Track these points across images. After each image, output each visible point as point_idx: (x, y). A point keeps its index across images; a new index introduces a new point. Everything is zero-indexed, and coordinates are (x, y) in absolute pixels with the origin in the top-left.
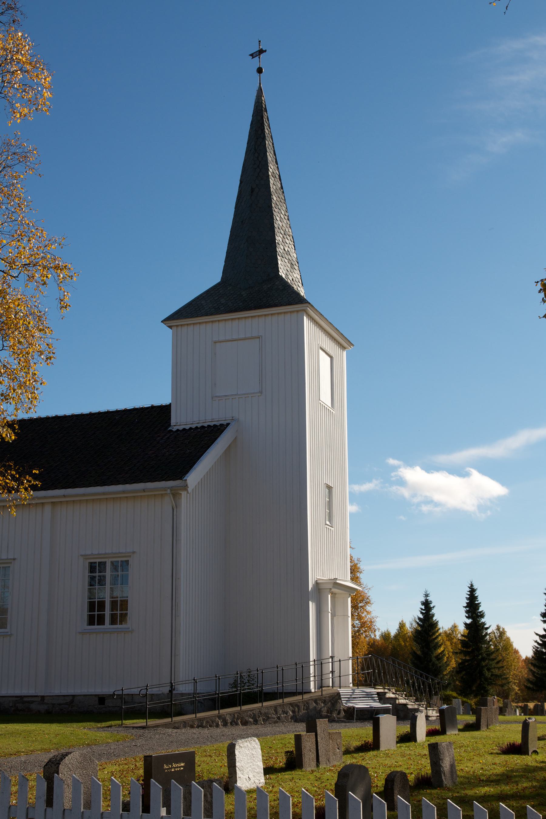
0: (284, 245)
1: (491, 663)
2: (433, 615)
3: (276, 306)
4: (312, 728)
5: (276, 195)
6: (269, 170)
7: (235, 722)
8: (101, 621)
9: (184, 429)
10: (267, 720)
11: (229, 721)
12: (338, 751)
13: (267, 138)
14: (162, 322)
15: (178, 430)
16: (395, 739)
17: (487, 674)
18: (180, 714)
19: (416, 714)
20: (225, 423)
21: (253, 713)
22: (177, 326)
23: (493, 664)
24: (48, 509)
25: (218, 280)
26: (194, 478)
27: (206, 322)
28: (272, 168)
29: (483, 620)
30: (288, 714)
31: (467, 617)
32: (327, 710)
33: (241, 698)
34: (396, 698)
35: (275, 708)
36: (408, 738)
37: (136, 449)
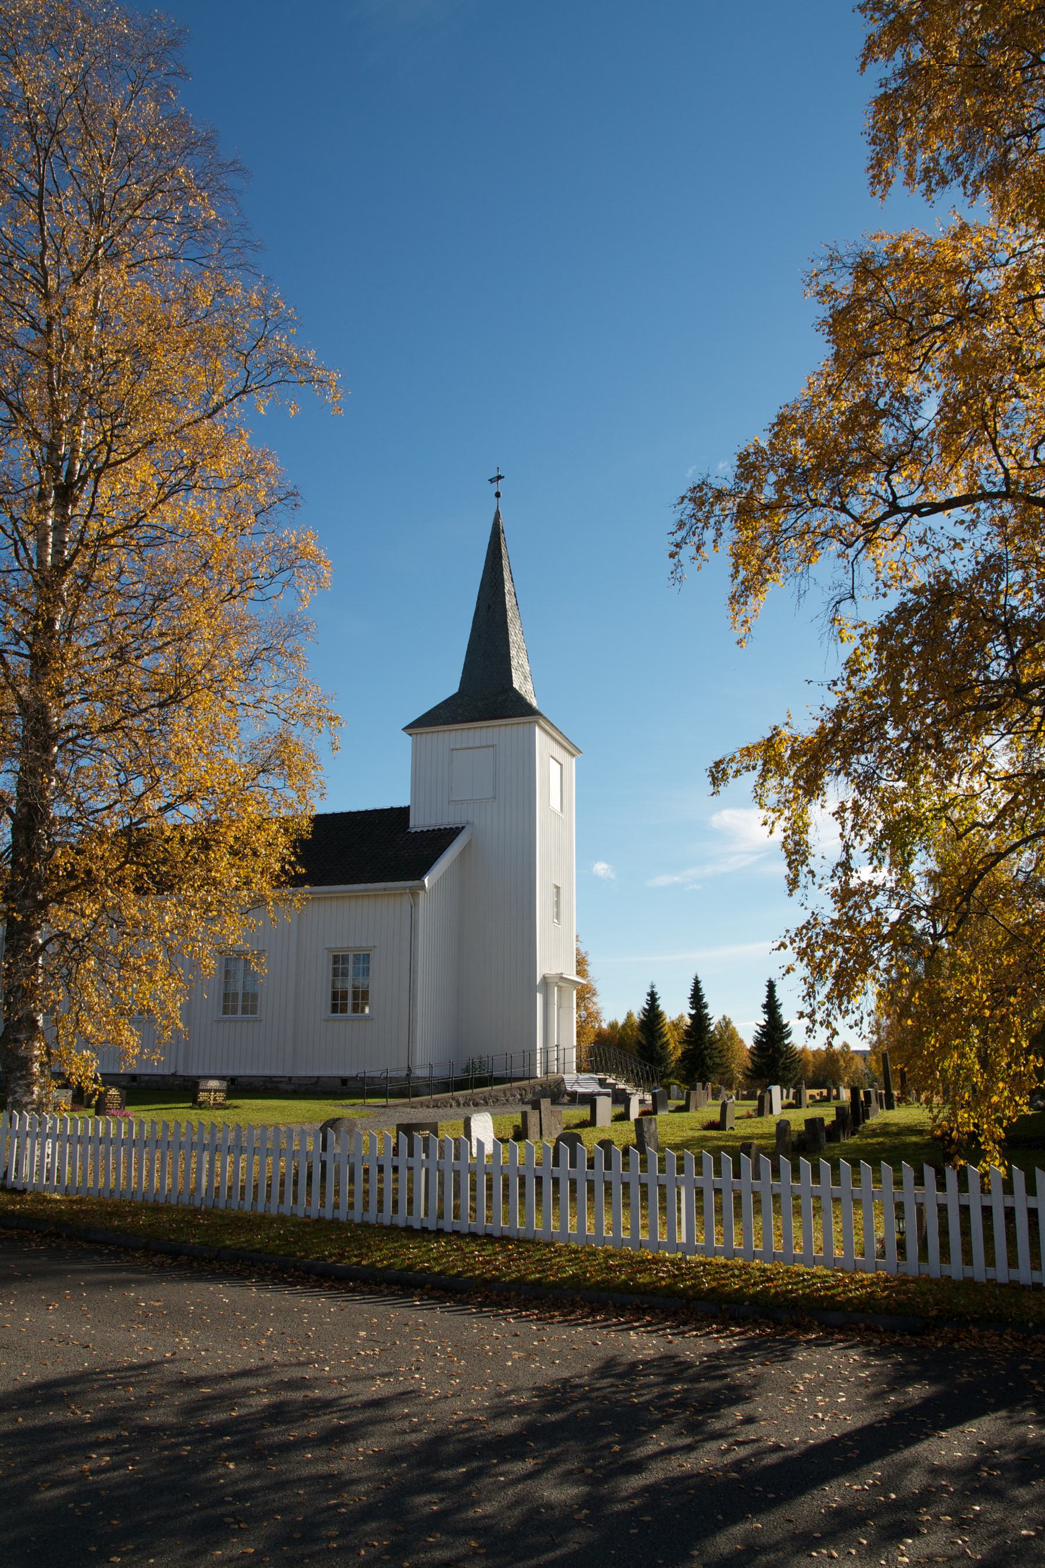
0: (519, 659)
3: (510, 717)
4: (536, 1106)
8: (344, 1010)
11: (462, 1102)
16: (610, 1118)
17: (709, 1062)
20: (460, 826)
23: (715, 1053)
28: (508, 586)
33: (473, 1080)
36: (623, 1117)
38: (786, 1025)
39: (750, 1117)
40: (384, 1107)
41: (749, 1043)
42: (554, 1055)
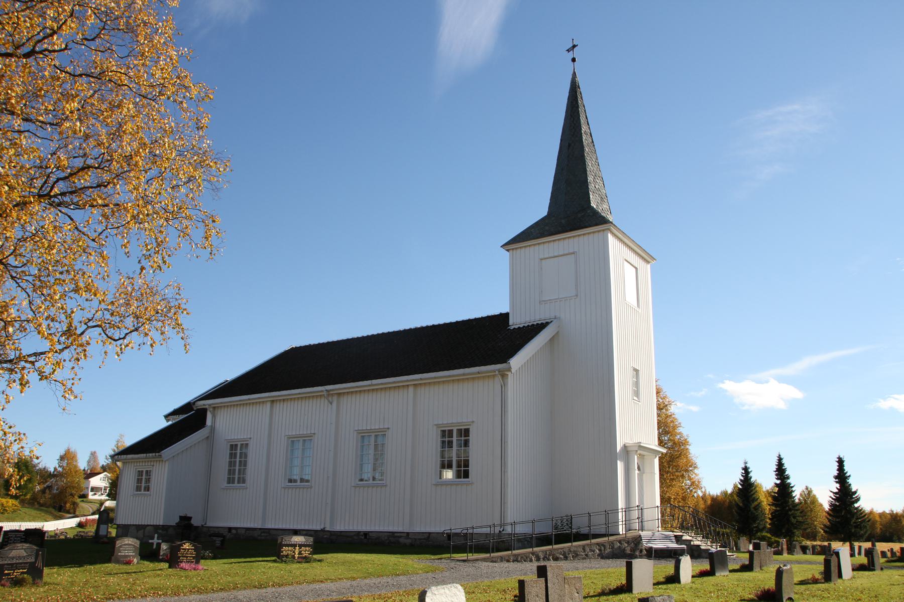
11: (542, 557)
17: (793, 521)
18: (498, 550)
23: (798, 513)
24: (411, 389)
26: (516, 362)
28: (584, 128)
29: (789, 481)
37: (483, 343)
38: (855, 492)
39: (815, 581)
40: (464, 561)
41: (827, 507)
42: (635, 514)
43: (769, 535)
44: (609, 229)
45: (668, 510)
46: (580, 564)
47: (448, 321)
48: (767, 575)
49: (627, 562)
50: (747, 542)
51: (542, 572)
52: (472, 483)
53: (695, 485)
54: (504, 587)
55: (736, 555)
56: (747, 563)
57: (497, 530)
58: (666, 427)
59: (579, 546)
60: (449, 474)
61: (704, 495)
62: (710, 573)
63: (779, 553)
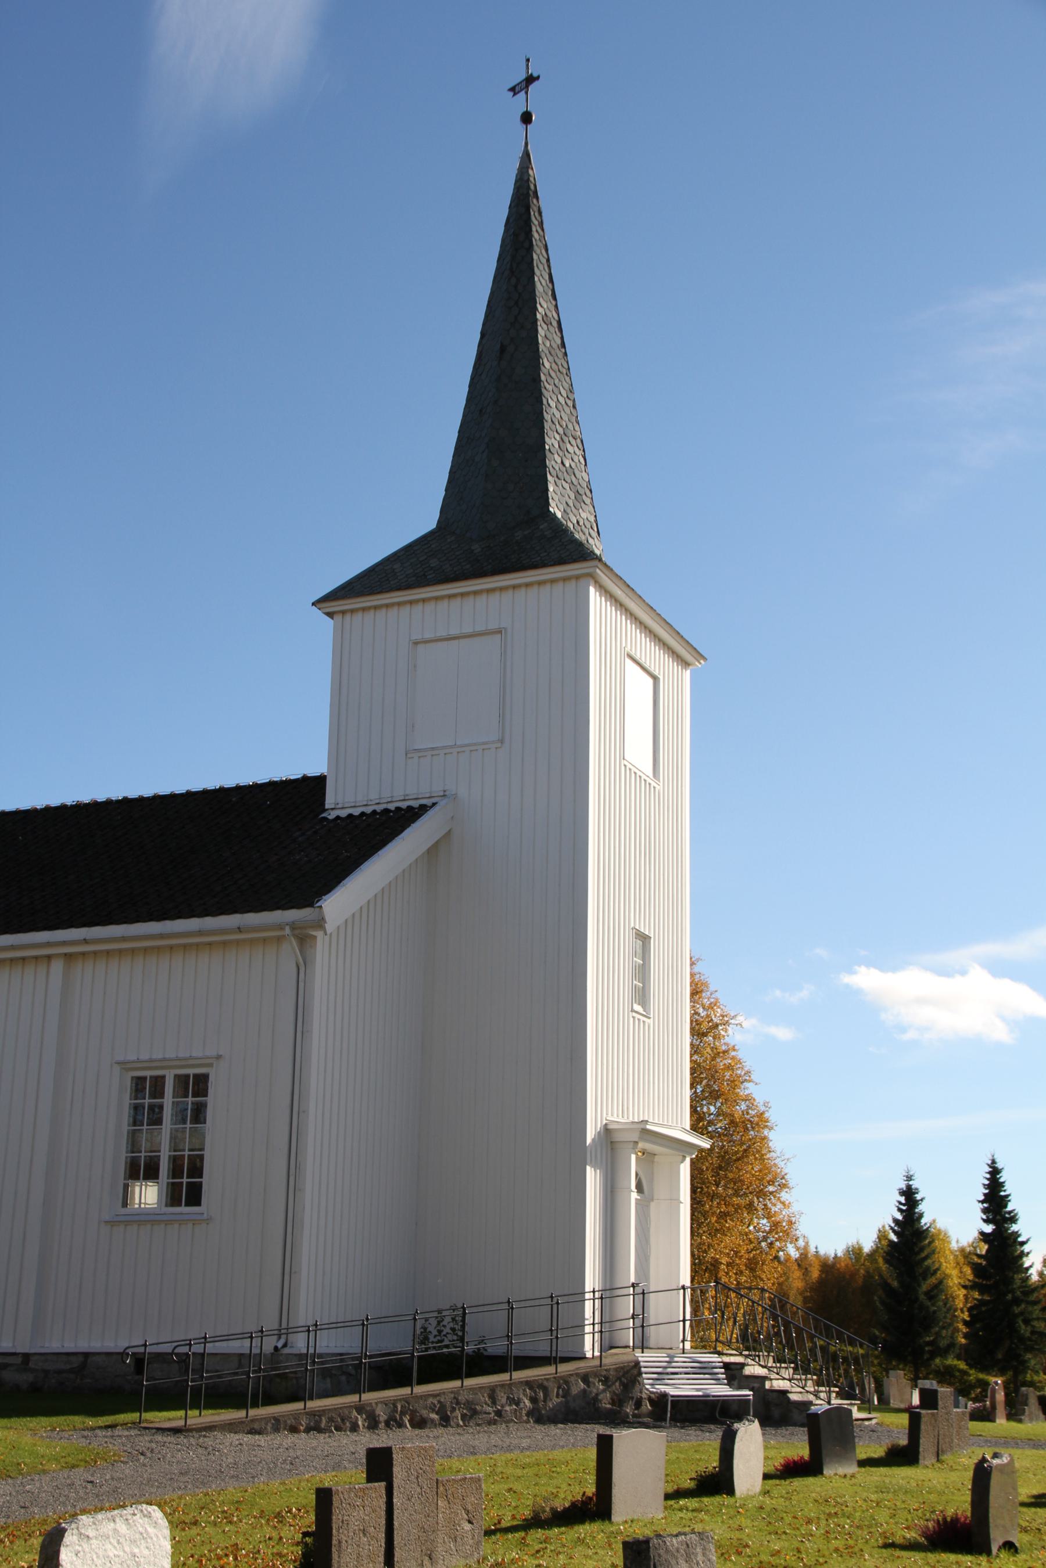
1: (1030, 1309)
2: (921, 1215)
5: (551, 358)
6: (536, 309)
7: (395, 1420)
9: (350, 816)
10: (471, 1417)
11: (383, 1417)
12: (467, 1527)
13: (535, 248)
14: (313, 604)
15: (338, 818)
17: (1024, 1330)
19: (736, 1425)
21: (439, 1402)
22: (343, 612)
23: (1036, 1311)
24: (57, 967)
25: (432, 525)
26: (339, 904)
27: (399, 604)
28: (543, 306)
29: (1014, 1228)
30: (522, 1405)
31: (985, 1221)
32: (612, 1399)
34: (763, 1379)
35: (492, 1393)
37: (252, 852)
40: (176, 1431)
41: (588, 1168)
42: (627, 1306)
43: (962, 1365)
44: (592, 576)
45: (711, 1293)
46: (478, 1437)
47: (164, 790)
48: (953, 1477)
49: (600, 1437)
50: (905, 1383)
51: (379, 1465)
52: (208, 1220)
53: (783, 1230)
54: (277, 1504)
55: (877, 1417)
56: (904, 1441)
57: (269, 1344)
58: (713, 1081)
59: (481, 1388)
60: (148, 1195)
61: (804, 1255)
62: (809, 1468)
63: (985, 1415)
